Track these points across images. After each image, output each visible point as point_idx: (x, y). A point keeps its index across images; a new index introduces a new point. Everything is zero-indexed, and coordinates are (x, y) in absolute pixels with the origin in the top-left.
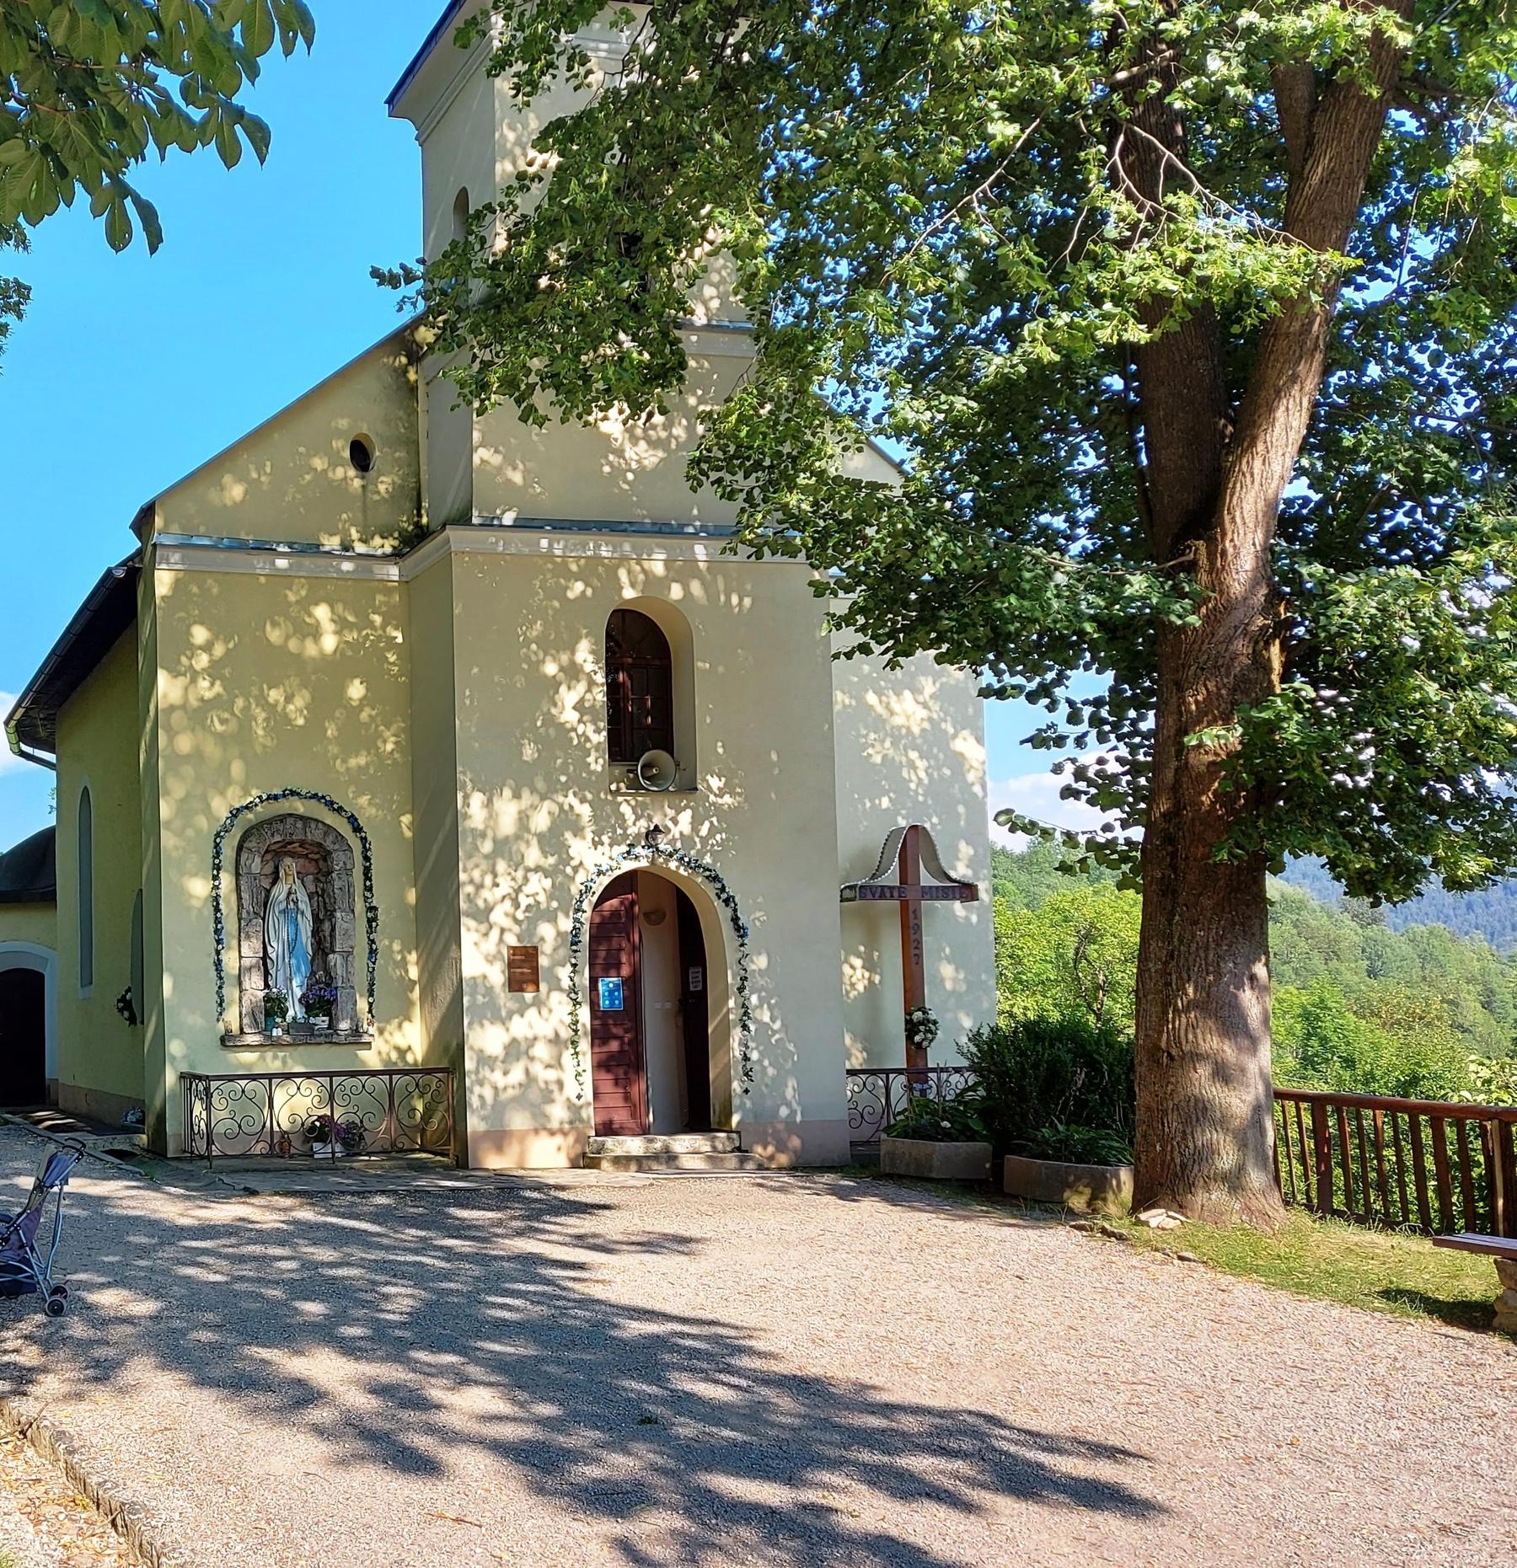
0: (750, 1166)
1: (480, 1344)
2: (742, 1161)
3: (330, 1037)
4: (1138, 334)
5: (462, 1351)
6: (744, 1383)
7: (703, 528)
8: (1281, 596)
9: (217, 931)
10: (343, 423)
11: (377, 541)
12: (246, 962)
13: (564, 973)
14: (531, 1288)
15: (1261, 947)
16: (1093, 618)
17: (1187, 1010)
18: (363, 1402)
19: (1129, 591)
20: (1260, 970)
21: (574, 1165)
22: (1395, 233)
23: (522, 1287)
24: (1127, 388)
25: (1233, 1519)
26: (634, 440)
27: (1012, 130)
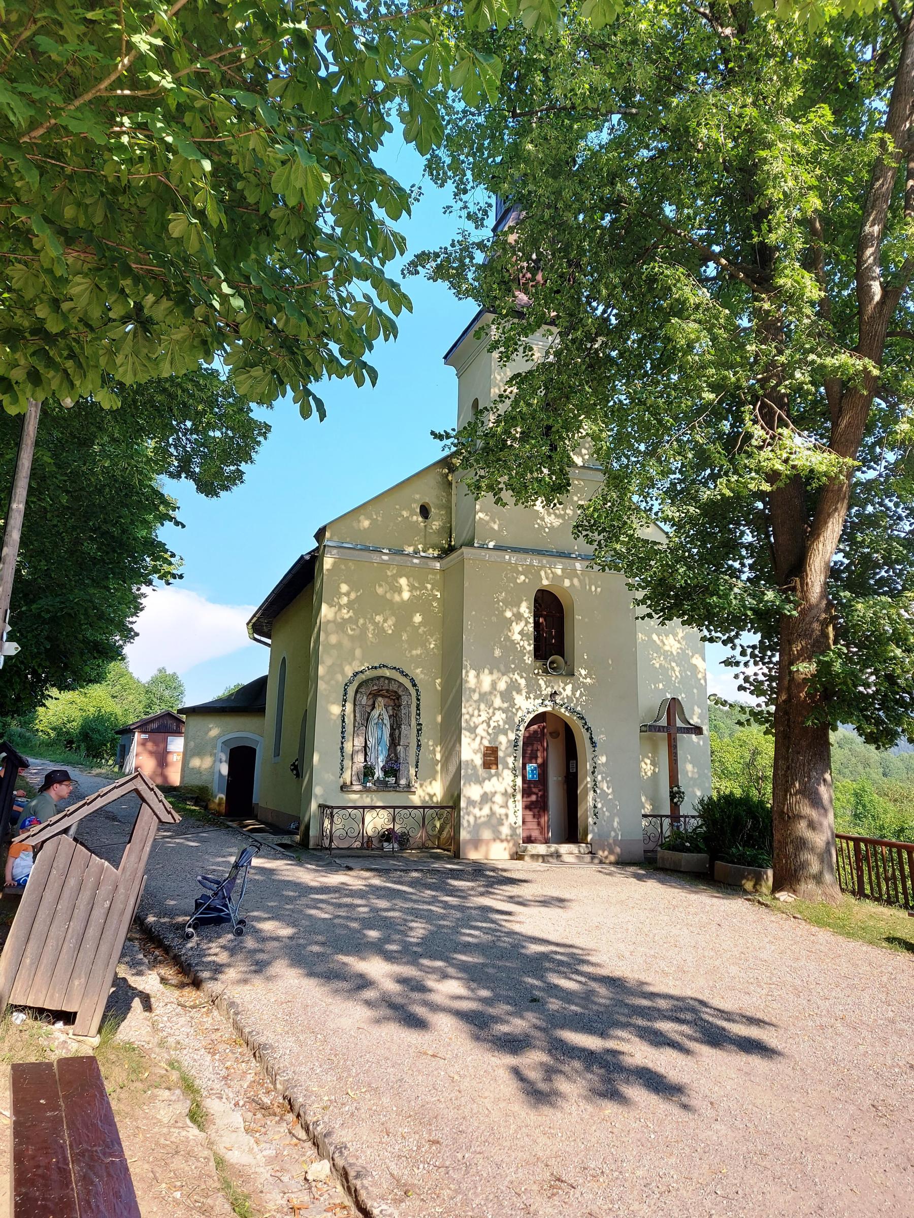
0: (596, 861)
1: (455, 956)
2: (592, 858)
3: (396, 787)
4: (766, 487)
5: (447, 959)
6: (583, 979)
7: (580, 555)
8: (833, 605)
9: (343, 732)
10: (417, 496)
11: (431, 551)
12: (356, 748)
13: (510, 760)
14: (484, 925)
15: (828, 766)
16: (751, 609)
17: (796, 794)
18: (391, 987)
19: (766, 598)
20: (827, 776)
21: (512, 858)
22: (878, 450)
23: (480, 924)
24: (765, 508)
25: (813, 1060)
26: (549, 514)
27: (712, 396)
